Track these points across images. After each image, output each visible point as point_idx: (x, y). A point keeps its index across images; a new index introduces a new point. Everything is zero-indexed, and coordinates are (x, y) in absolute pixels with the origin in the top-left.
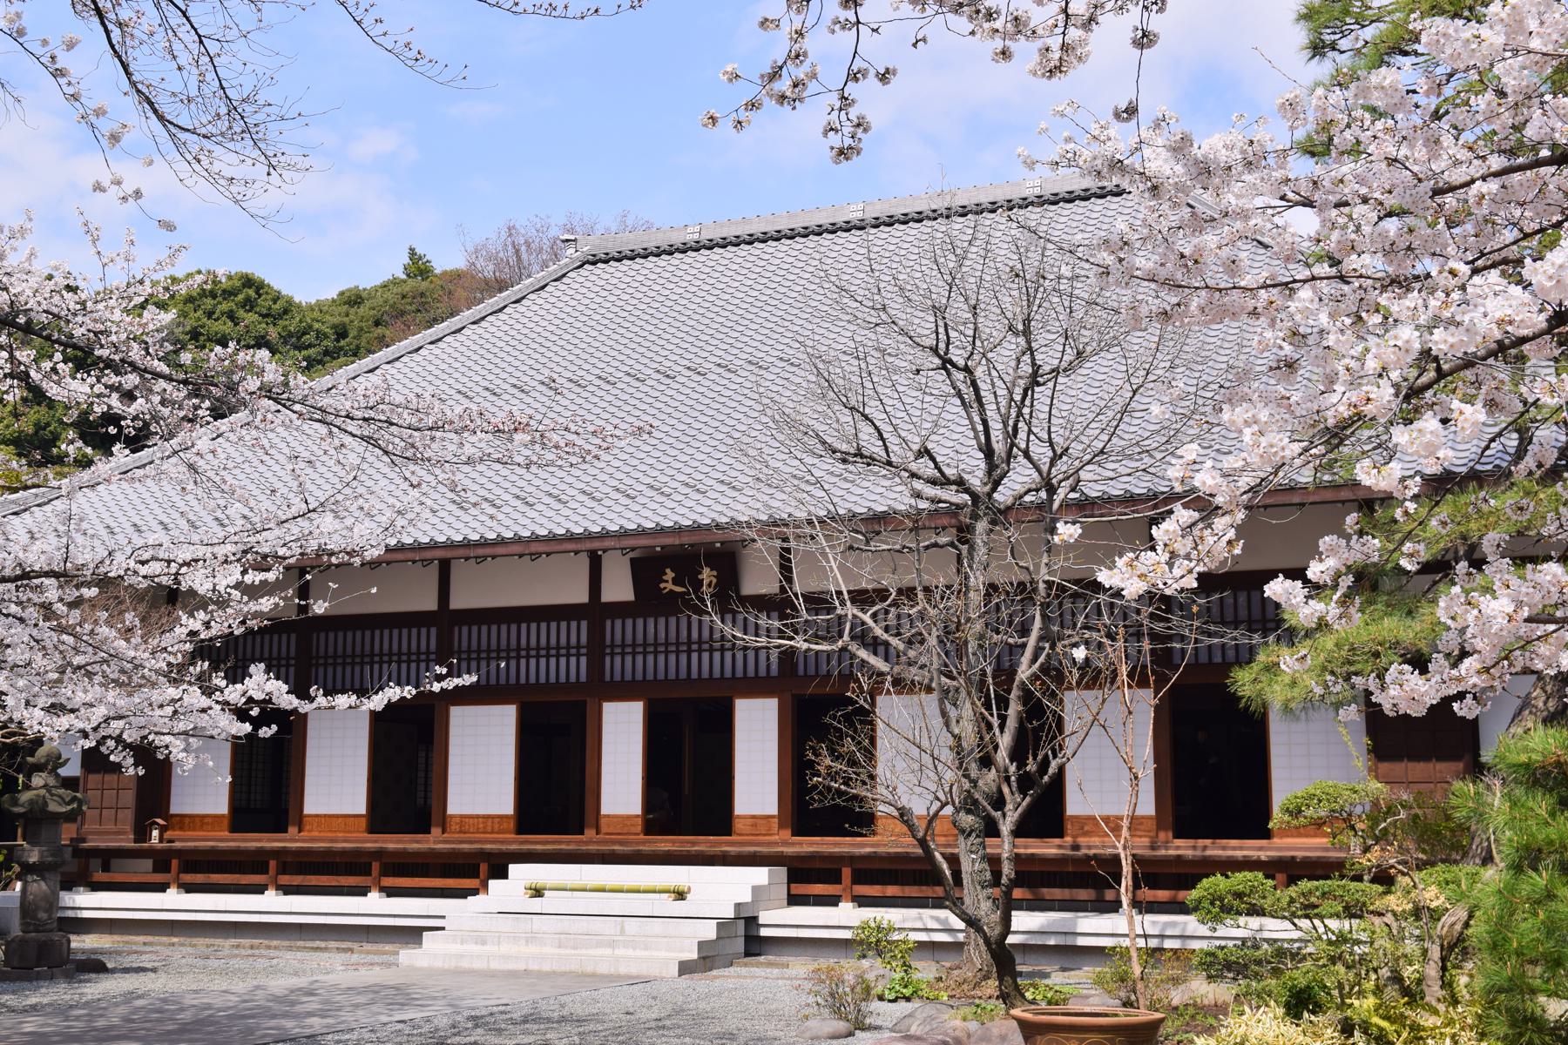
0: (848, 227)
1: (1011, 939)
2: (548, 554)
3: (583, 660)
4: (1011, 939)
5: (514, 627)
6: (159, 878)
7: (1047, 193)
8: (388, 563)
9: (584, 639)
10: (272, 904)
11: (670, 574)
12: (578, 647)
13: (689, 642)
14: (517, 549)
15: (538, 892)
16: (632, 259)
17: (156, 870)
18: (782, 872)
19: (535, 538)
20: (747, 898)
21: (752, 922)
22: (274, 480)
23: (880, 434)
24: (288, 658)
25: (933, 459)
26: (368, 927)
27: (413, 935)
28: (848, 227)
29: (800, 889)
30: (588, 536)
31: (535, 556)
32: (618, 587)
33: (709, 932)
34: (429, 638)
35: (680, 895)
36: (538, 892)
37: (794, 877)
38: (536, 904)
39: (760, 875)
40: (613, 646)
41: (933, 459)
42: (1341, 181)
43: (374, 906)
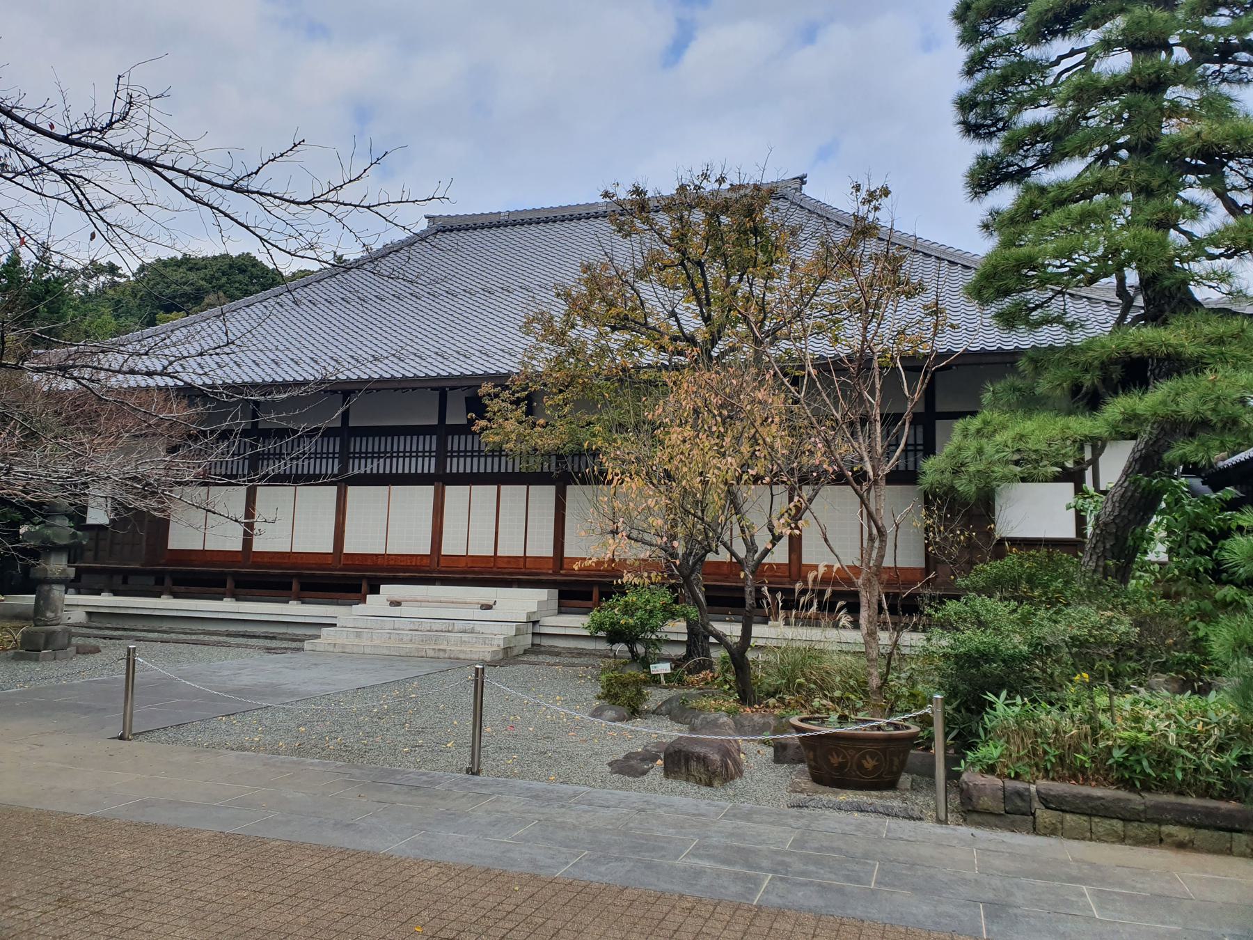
2: (378, 390)
3: (433, 460)
5: (389, 439)
6: (158, 588)
8: (378, 390)
10: (227, 607)
15: (396, 603)
17: (156, 584)
18: (556, 592)
19: (244, 384)
23: (293, 202)
24: (334, 453)
25: (677, 320)
30: (439, 378)
31: (405, 389)
36: (396, 603)
37: (562, 596)
38: (396, 611)
39: (542, 594)
41: (677, 320)
42: (571, 758)
43: (294, 610)
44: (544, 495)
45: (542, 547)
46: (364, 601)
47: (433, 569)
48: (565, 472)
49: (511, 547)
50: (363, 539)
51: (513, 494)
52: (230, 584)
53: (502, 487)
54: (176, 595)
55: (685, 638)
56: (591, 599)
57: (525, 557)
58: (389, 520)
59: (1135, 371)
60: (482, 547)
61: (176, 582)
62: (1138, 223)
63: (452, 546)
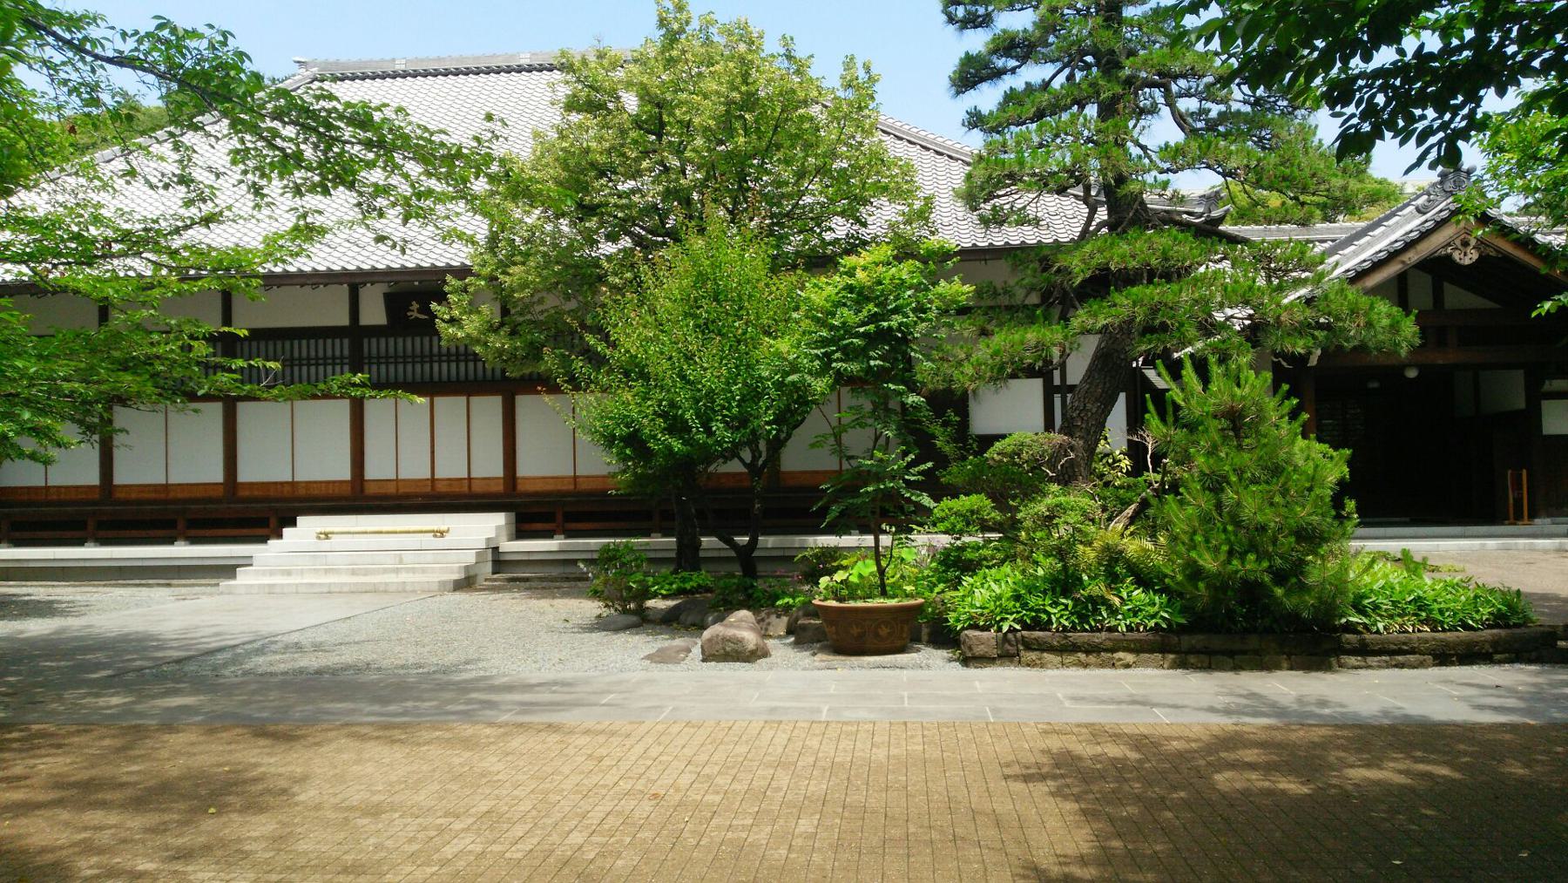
0: (520, 69)
1: (755, 554)
4: (755, 554)
7: (535, 63)
9: (346, 352)
10: (182, 551)
11: (415, 306)
12: (342, 357)
13: (431, 355)
14: (303, 280)
16: (394, 77)
20: (492, 535)
21: (496, 549)
22: (1411, 208)
24: (342, 357)
26: (120, 568)
27: (227, 570)
28: (520, 69)
29: (527, 527)
31: (315, 285)
32: (374, 313)
33: (470, 558)
34: (343, 347)
35: (442, 533)
38: (325, 545)
40: (370, 357)
44: (489, 408)
45: (489, 466)
46: (280, 536)
47: (357, 497)
48: (508, 385)
49: (451, 467)
50: (262, 465)
51: (450, 407)
52: (181, 525)
53: (437, 400)
54: (194, 540)
55: (673, 555)
56: (85, 528)
57: (575, 477)
58: (296, 440)
59: (1102, 283)
60: (415, 468)
61: (101, 525)
62: (329, 142)
63: (378, 468)
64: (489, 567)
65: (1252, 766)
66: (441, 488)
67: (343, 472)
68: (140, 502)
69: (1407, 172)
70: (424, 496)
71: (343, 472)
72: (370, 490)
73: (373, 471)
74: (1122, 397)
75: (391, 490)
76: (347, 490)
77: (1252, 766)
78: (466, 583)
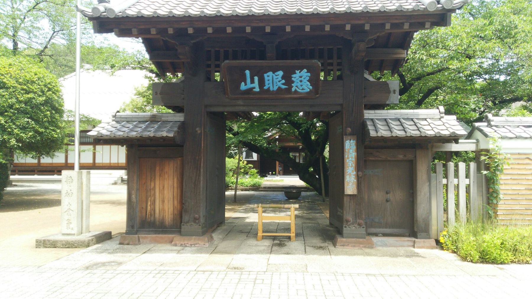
10: (36, 177)
49: (114, 161)
52: (36, 171)
60: (106, 161)
61: (19, 171)
63: (98, 161)
64: (120, 181)
65: (241, 105)
66: (112, 165)
67: (91, 161)
68: (46, 167)
69: (104, 24)
70: (108, 166)
71: (91, 161)
72: (97, 165)
73: (97, 161)
74: (277, 163)
75: (101, 165)
76: (91, 165)
77: (241, 105)
78: (115, 183)
